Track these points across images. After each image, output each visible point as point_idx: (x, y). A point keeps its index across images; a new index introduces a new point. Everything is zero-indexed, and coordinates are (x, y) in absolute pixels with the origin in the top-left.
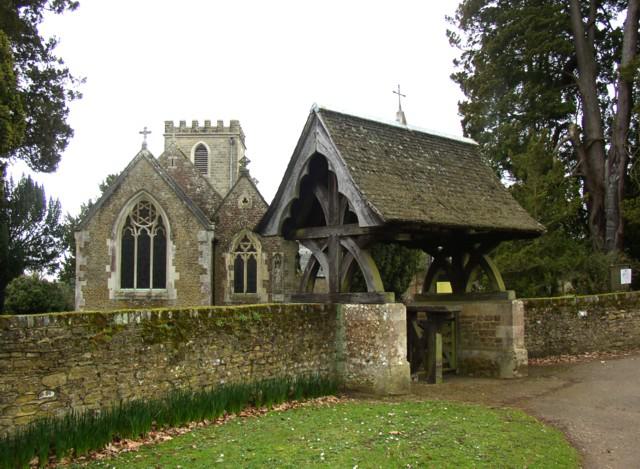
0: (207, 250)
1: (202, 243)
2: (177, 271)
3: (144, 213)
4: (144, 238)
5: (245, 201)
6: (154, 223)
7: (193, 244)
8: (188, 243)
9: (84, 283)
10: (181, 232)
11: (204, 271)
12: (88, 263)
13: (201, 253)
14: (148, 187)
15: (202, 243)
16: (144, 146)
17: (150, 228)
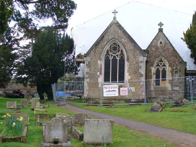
0: (143, 66)
1: (141, 62)
2: (129, 75)
3: (115, 49)
4: (115, 60)
5: (161, 43)
6: (119, 53)
7: (137, 63)
8: (134, 62)
9: (88, 80)
10: (132, 57)
11: (142, 75)
12: (90, 71)
13: (141, 67)
14: (116, 37)
15: (141, 62)
16: (115, 18)
17: (117, 55)
